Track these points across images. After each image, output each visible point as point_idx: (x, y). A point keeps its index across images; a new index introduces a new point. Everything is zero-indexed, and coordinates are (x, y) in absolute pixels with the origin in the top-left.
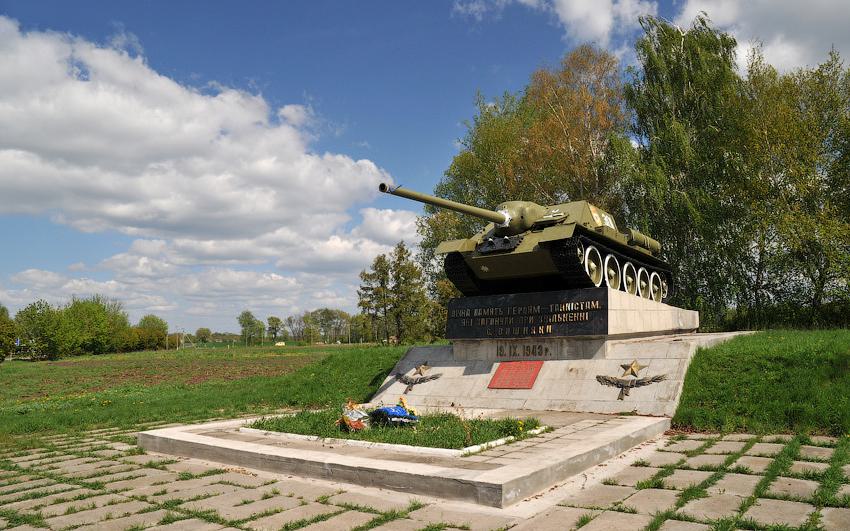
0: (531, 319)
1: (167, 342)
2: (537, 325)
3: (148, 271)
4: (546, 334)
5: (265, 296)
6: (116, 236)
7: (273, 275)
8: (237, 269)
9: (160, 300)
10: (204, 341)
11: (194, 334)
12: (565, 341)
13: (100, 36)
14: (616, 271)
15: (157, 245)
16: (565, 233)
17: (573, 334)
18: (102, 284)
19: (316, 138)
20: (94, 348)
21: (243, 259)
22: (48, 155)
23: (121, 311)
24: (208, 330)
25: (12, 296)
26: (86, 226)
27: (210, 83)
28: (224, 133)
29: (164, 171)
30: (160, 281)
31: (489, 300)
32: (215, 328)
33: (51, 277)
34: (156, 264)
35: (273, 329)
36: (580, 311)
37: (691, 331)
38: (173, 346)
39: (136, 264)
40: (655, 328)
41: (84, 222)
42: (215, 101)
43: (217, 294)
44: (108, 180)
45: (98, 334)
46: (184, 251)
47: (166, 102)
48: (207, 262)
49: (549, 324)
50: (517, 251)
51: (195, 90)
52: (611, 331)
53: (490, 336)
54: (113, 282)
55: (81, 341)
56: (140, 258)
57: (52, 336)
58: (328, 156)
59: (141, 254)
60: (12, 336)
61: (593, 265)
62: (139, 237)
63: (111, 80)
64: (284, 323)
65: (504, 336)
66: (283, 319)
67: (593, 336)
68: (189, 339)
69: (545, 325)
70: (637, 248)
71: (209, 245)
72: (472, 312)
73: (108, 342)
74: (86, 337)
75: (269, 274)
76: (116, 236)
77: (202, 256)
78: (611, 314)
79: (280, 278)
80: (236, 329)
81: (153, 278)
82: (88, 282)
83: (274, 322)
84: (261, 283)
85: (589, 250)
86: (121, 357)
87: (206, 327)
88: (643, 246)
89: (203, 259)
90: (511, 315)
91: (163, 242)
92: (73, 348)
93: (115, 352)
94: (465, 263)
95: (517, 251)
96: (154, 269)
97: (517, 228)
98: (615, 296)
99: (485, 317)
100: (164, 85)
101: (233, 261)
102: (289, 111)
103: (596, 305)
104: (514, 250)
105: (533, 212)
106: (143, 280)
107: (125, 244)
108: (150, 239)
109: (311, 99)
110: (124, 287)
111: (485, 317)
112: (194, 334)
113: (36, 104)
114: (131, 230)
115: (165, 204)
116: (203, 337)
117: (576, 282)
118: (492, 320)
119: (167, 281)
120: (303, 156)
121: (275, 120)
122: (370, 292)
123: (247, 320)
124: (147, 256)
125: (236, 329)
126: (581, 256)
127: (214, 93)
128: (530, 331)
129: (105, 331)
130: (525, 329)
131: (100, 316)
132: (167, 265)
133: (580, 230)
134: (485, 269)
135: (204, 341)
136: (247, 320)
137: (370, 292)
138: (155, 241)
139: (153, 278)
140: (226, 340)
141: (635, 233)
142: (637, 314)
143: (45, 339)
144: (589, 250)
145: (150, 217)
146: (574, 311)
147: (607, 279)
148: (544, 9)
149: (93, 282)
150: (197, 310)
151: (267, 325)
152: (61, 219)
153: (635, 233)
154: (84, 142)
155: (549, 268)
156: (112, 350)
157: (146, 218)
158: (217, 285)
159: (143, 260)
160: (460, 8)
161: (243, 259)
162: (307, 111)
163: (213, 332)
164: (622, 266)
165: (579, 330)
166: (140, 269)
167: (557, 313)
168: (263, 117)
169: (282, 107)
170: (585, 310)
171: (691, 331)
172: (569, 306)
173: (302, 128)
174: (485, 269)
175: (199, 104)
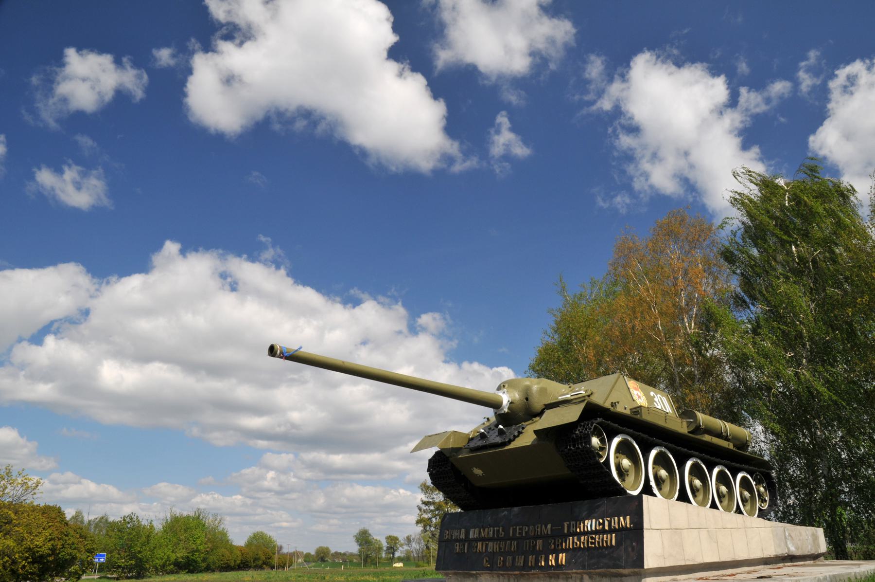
0: (539, 543)
1: (275, 561)
2: (547, 553)
3: (275, 486)
4: (558, 566)
5: (392, 513)
6: (247, 449)
7: (402, 491)
8: (364, 483)
9: (285, 516)
10: (323, 560)
11: (313, 553)
12: (586, 577)
13: (252, 253)
14: (670, 470)
15: (285, 459)
16: (571, 414)
17: (590, 567)
18: (228, 499)
19: (454, 344)
20: (188, 566)
21: (371, 474)
22: (191, 367)
23: (222, 526)
24: (327, 549)
25: (143, 510)
26: (218, 439)
27: (352, 292)
28: (364, 343)
29: (304, 382)
30: (286, 496)
31: (489, 516)
32: (336, 546)
33: (181, 491)
34: (283, 478)
35: (392, 549)
36: (603, 531)
37: (814, 557)
38: (282, 566)
39: (262, 478)
40: (742, 556)
41: (216, 434)
42: (357, 310)
43: (344, 510)
44: (245, 393)
45: (193, 551)
46: (312, 466)
47: (308, 312)
48: (333, 477)
49: (562, 551)
50: (513, 445)
51: (338, 299)
52: (650, 562)
53: (487, 569)
54: (239, 497)
55: (173, 557)
56: (268, 472)
57: (140, 552)
58: (466, 365)
59: (269, 468)
60: (90, 551)
61: (626, 463)
62: (268, 450)
63: (260, 295)
64: (402, 542)
65: (504, 568)
66: (402, 537)
67: (621, 571)
68: (307, 558)
69: (556, 552)
70: (707, 438)
71: (338, 459)
72: (467, 533)
73: (204, 560)
74: (180, 554)
75: (396, 489)
76: (247, 449)
77: (330, 470)
78: (647, 535)
79: (409, 493)
80: (353, 548)
81: (278, 493)
82: (216, 496)
83: (393, 542)
84: (389, 498)
85: (653, 453)
86: (216, 576)
87: (325, 546)
88: (719, 435)
89: (333, 476)
90: (513, 538)
91: (291, 456)
92: (163, 566)
93: (213, 571)
94: (453, 465)
95: (513, 445)
96: (281, 484)
97: (521, 414)
98: (658, 511)
99: (483, 540)
100: (309, 296)
101: (362, 476)
102: (426, 319)
103: (626, 521)
104: (510, 442)
105: (543, 391)
106: (269, 495)
107: (255, 458)
108: (279, 453)
109: (450, 305)
110: (249, 501)
111: (483, 540)
112: (313, 553)
113: (188, 318)
114: (262, 443)
115: (295, 416)
116: (322, 556)
117: (596, 488)
118: (490, 544)
119: (294, 496)
120: (442, 364)
121: (414, 330)
122: (432, 508)
123: (364, 538)
124: (275, 471)
125: (353, 548)
126: (602, 449)
127: (356, 302)
128: (537, 561)
129: (201, 548)
130: (532, 558)
131: (198, 533)
132: (293, 480)
133: (592, 411)
134: (478, 472)
135: (323, 560)
136: (364, 538)
137: (432, 508)
138: (283, 455)
139: (278, 493)
140: (345, 559)
141: (702, 418)
142: (704, 533)
143: (133, 556)
144: (616, 440)
145: (282, 429)
146: (596, 532)
147: (653, 483)
148: (691, 200)
149: (221, 497)
150: (321, 527)
151: (385, 544)
152: (195, 431)
153: (702, 418)
154: (226, 355)
155: (556, 468)
156: (208, 569)
157: (278, 430)
158: (344, 501)
159: (271, 474)
160: (601, 204)
161: (371, 474)
162: (445, 319)
163: (333, 551)
164: (681, 466)
165: (605, 561)
166: (266, 484)
167: (575, 534)
168: (403, 326)
169: (419, 317)
170: (611, 531)
171: (814, 557)
172: (590, 524)
173: (440, 336)
174: (478, 472)
175: (339, 313)
